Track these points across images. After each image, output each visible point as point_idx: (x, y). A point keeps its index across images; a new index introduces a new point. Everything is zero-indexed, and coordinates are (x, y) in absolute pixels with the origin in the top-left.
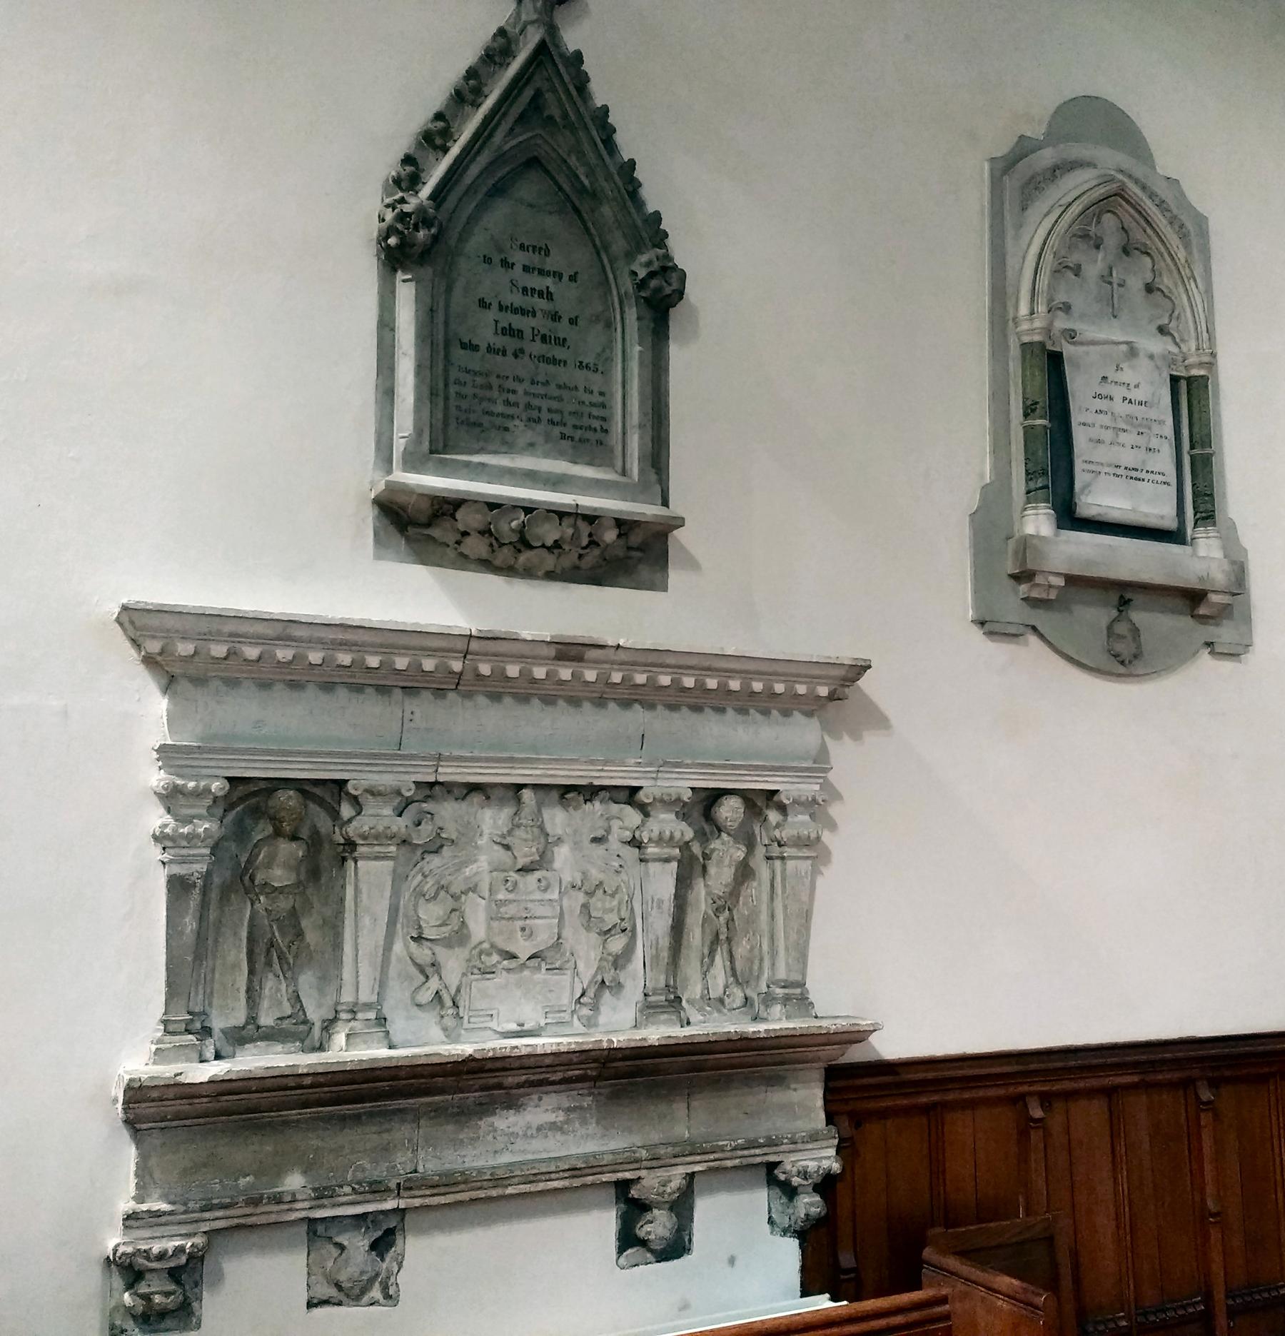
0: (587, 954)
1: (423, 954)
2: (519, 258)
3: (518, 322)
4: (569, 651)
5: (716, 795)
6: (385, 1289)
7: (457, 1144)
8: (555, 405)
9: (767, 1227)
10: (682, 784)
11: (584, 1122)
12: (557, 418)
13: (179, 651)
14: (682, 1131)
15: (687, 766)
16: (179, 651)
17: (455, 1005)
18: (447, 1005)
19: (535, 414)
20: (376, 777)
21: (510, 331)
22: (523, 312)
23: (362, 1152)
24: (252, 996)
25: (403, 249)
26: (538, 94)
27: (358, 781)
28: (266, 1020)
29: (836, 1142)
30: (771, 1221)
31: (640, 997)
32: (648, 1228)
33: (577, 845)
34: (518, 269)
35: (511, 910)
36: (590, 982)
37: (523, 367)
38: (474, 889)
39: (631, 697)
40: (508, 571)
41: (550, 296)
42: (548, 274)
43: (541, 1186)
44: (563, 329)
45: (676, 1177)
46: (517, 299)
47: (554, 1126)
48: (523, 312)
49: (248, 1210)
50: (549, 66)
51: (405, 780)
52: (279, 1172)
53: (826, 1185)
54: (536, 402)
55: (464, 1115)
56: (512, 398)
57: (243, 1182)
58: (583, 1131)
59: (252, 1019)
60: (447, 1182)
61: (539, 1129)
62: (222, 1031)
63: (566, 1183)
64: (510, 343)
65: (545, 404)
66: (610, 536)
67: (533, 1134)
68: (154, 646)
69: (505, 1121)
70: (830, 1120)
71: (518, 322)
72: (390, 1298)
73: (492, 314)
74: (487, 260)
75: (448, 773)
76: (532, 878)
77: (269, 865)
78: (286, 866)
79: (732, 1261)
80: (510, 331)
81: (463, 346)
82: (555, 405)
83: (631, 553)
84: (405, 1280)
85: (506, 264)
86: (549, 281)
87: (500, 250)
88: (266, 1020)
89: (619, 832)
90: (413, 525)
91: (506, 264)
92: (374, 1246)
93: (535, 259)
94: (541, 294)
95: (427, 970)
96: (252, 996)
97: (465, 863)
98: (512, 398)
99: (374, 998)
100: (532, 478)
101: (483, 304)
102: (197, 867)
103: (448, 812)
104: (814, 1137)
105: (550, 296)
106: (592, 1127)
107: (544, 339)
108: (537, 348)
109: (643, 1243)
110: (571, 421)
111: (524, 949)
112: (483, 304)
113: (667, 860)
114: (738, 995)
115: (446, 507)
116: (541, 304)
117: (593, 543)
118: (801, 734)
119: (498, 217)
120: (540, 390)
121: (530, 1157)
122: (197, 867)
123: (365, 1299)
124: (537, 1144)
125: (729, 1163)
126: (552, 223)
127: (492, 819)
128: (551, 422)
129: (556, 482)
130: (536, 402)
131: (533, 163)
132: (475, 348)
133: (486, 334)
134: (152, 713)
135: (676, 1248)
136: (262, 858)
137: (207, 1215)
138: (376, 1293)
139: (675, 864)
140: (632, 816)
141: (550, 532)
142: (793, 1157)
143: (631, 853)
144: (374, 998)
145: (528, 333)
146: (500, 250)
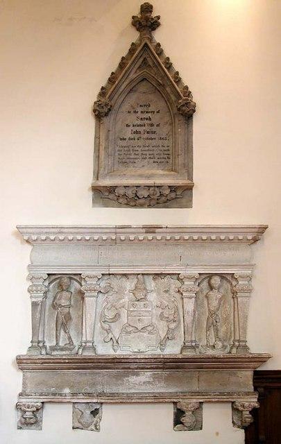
0: (162, 328)
1: (106, 326)
2: (139, 109)
3: (138, 129)
4: (150, 229)
5: (210, 276)
6: (96, 426)
7: (116, 385)
8: (151, 152)
9: (232, 425)
10: (195, 272)
11: (160, 382)
12: (152, 156)
13: (30, 237)
14: (195, 388)
15: (197, 266)
16: (30, 237)
17: (117, 342)
18: (115, 342)
19: (145, 156)
20: (90, 272)
21: (136, 132)
22: (141, 125)
23: (104, 381)
24: (57, 338)
25: (101, 112)
26: (145, 59)
27: (85, 273)
28: (61, 344)
29: (257, 396)
30: (233, 422)
31: (183, 344)
32: (183, 418)
33: (159, 294)
34: (139, 113)
35: (135, 314)
36: (165, 338)
37: (141, 143)
38: (123, 307)
39: (177, 242)
40: (135, 206)
41: (150, 119)
42: (149, 112)
43: (144, 401)
44: (154, 129)
45: (194, 401)
46: (139, 122)
47: (149, 382)
48: (141, 125)
49: (53, 397)
50: (148, 50)
51: (98, 273)
52: (62, 388)
53: (254, 412)
54: (144, 152)
55: (119, 377)
56: (137, 153)
57: (52, 389)
58: (159, 385)
59: (57, 344)
60: (112, 395)
61: (144, 383)
62: (50, 347)
63: (153, 400)
64: (137, 136)
65: (148, 153)
66: (167, 192)
67: (141, 382)
68: (26, 238)
69: (133, 379)
70: (256, 389)
71: (138, 129)
72: (97, 430)
73: (131, 128)
74: (129, 112)
75: (112, 271)
76: (142, 303)
77: (60, 299)
78: (65, 299)
79: (217, 434)
80: (136, 132)
81: (121, 139)
82: (151, 152)
83: (179, 195)
84: (102, 425)
85: (135, 112)
86: (150, 115)
87: (134, 108)
88: (61, 344)
89: (173, 288)
90: (104, 195)
91: (135, 112)
92: (92, 412)
93: (145, 109)
94: (147, 119)
95: (108, 331)
96: (57, 338)
97: (120, 299)
98: (137, 153)
99: (91, 339)
100: (141, 176)
101: (128, 126)
102: (39, 299)
103: (115, 282)
104: (247, 394)
105: (150, 119)
106: (163, 384)
107: (148, 133)
108: (146, 136)
109: (182, 423)
110: (157, 157)
111: (140, 326)
112: (128, 126)
113: (190, 298)
114: (220, 344)
115: (112, 189)
116: (148, 122)
117: (161, 195)
118: (242, 254)
119: (133, 99)
120: (147, 148)
121: (141, 391)
122: (39, 299)
123: (89, 428)
124: (143, 387)
125: (213, 400)
126: (151, 97)
127: (129, 285)
128: (150, 158)
129: (148, 177)
130: (144, 152)
131: (144, 79)
132: (125, 139)
133: (129, 135)
134: (25, 254)
135: (197, 426)
136: (59, 294)
137: (41, 397)
138: (93, 428)
139: (194, 299)
140: (178, 284)
141: (145, 193)
142: (239, 400)
143: (178, 296)
144: (91, 339)
145: (142, 132)
146: (134, 108)
